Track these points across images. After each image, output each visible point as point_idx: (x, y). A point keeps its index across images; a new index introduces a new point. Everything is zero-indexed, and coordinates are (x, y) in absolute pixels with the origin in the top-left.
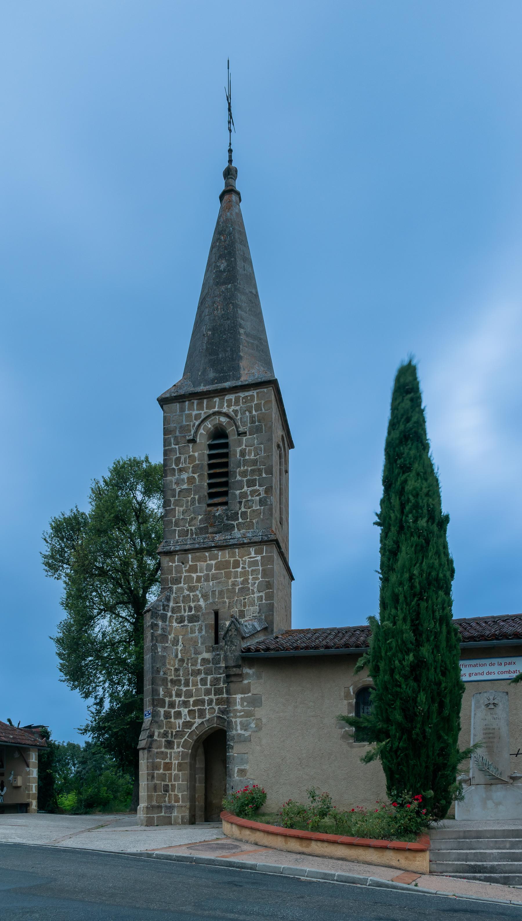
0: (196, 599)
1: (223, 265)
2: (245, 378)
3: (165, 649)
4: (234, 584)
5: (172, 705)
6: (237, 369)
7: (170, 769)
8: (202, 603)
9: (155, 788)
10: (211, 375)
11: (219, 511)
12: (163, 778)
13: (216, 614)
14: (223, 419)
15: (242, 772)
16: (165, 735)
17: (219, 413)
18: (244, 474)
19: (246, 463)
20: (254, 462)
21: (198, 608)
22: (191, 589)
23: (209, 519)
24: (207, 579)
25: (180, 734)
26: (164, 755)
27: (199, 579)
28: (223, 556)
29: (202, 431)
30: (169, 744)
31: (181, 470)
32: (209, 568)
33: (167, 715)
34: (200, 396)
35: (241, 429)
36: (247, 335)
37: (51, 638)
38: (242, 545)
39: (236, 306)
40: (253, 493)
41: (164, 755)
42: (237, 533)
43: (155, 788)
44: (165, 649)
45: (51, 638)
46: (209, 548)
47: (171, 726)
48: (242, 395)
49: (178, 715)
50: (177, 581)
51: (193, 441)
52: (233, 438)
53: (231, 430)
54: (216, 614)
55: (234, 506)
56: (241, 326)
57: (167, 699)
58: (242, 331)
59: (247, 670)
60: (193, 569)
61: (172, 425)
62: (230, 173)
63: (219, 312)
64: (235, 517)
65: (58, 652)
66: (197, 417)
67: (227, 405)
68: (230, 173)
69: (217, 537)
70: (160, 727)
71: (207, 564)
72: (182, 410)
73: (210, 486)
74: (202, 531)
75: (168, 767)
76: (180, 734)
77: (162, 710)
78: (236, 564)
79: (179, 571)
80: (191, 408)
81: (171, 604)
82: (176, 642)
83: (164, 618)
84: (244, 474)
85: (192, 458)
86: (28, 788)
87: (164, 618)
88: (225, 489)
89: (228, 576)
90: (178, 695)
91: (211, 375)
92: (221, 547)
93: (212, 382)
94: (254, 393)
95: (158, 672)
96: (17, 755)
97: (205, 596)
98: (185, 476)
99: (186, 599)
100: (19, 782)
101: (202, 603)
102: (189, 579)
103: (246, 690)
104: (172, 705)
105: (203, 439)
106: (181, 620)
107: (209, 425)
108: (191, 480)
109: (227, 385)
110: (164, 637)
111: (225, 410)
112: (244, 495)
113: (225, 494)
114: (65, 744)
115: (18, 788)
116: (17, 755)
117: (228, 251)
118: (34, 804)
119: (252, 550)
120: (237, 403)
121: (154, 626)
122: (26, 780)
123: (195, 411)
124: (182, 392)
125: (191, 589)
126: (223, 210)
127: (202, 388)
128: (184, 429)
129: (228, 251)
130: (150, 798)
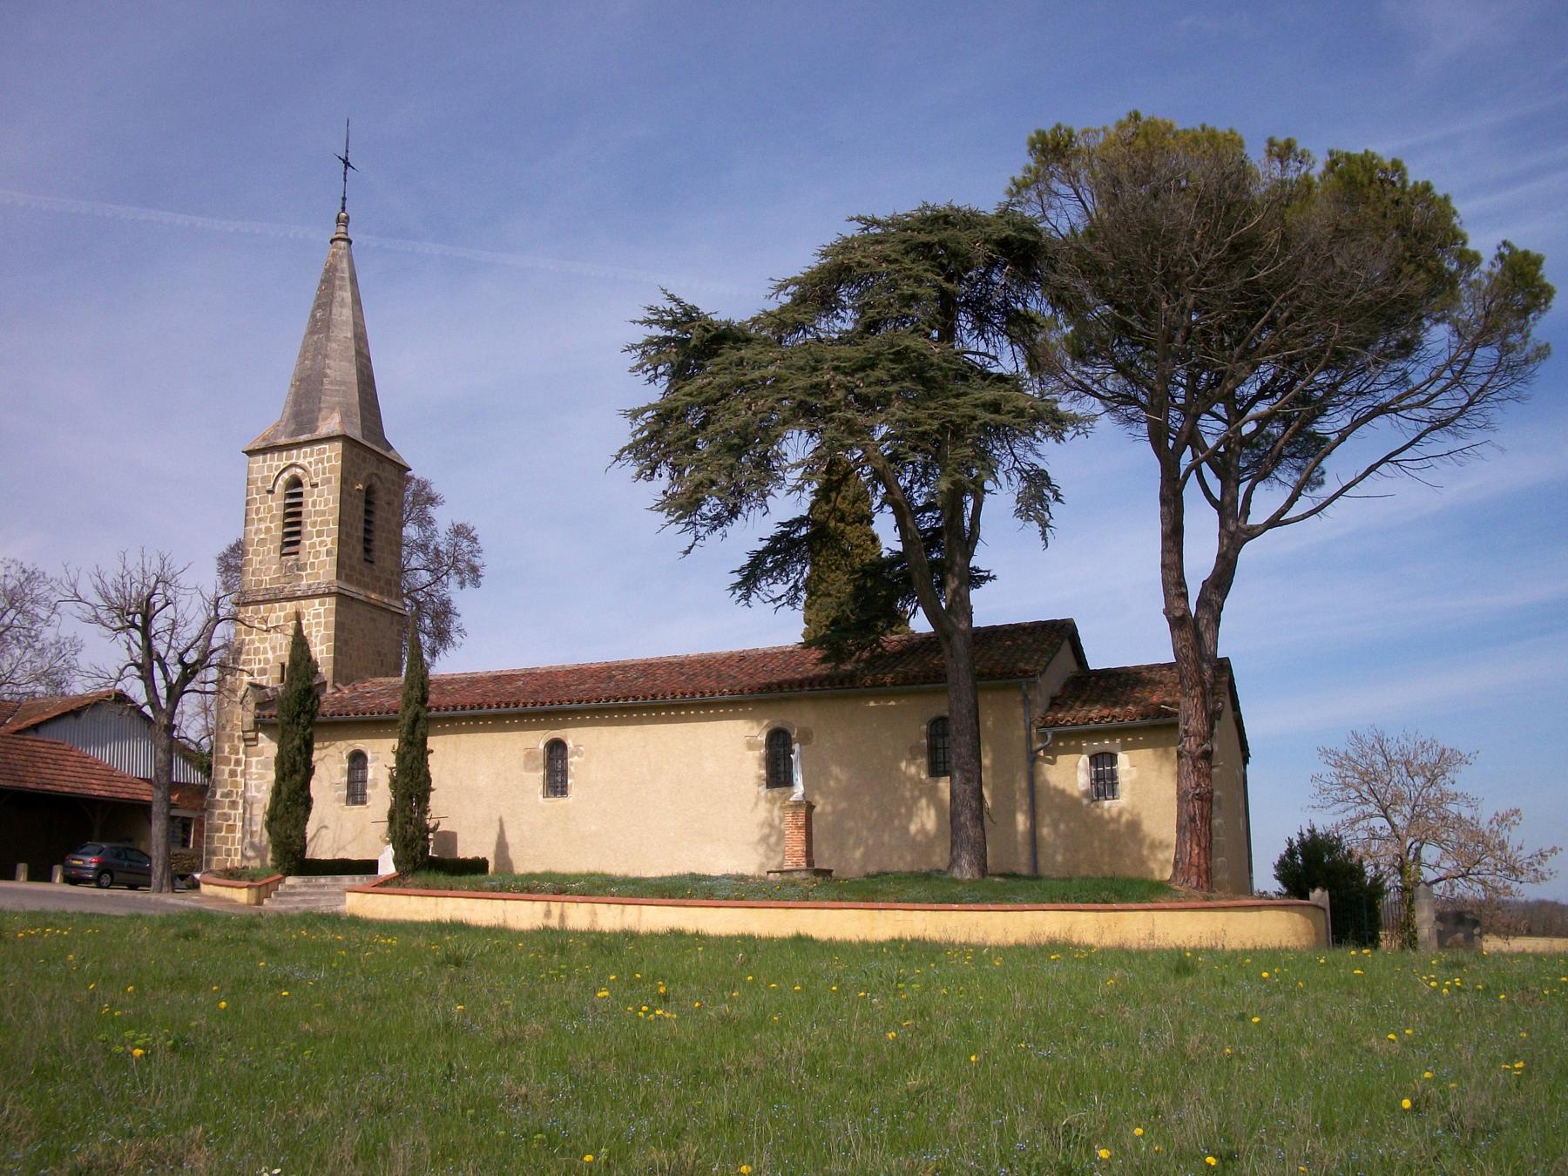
0: (265, 652)
7: (233, 831)
8: (270, 655)
14: (299, 471)
17: (292, 465)
18: (314, 524)
20: (323, 513)
21: (267, 661)
29: (280, 482)
31: (260, 520)
32: (278, 619)
35: (314, 480)
37: (687, 552)
45: (687, 552)
46: (278, 600)
52: (306, 488)
53: (305, 480)
55: (303, 557)
56: (326, 376)
57: (233, 757)
62: (665, 292)
65: (185, 617)
77: (227, 769)
85: (270, 509)
88: (286, 550)
95: (224, 728)
97: (273, 649)
98: (263, 526)
101: (270, 655)
107: (286, 475)
108: (268, 530)
109: (303, 438)
111: (300, 462)
112: (313, 546)
119: (317, 601)
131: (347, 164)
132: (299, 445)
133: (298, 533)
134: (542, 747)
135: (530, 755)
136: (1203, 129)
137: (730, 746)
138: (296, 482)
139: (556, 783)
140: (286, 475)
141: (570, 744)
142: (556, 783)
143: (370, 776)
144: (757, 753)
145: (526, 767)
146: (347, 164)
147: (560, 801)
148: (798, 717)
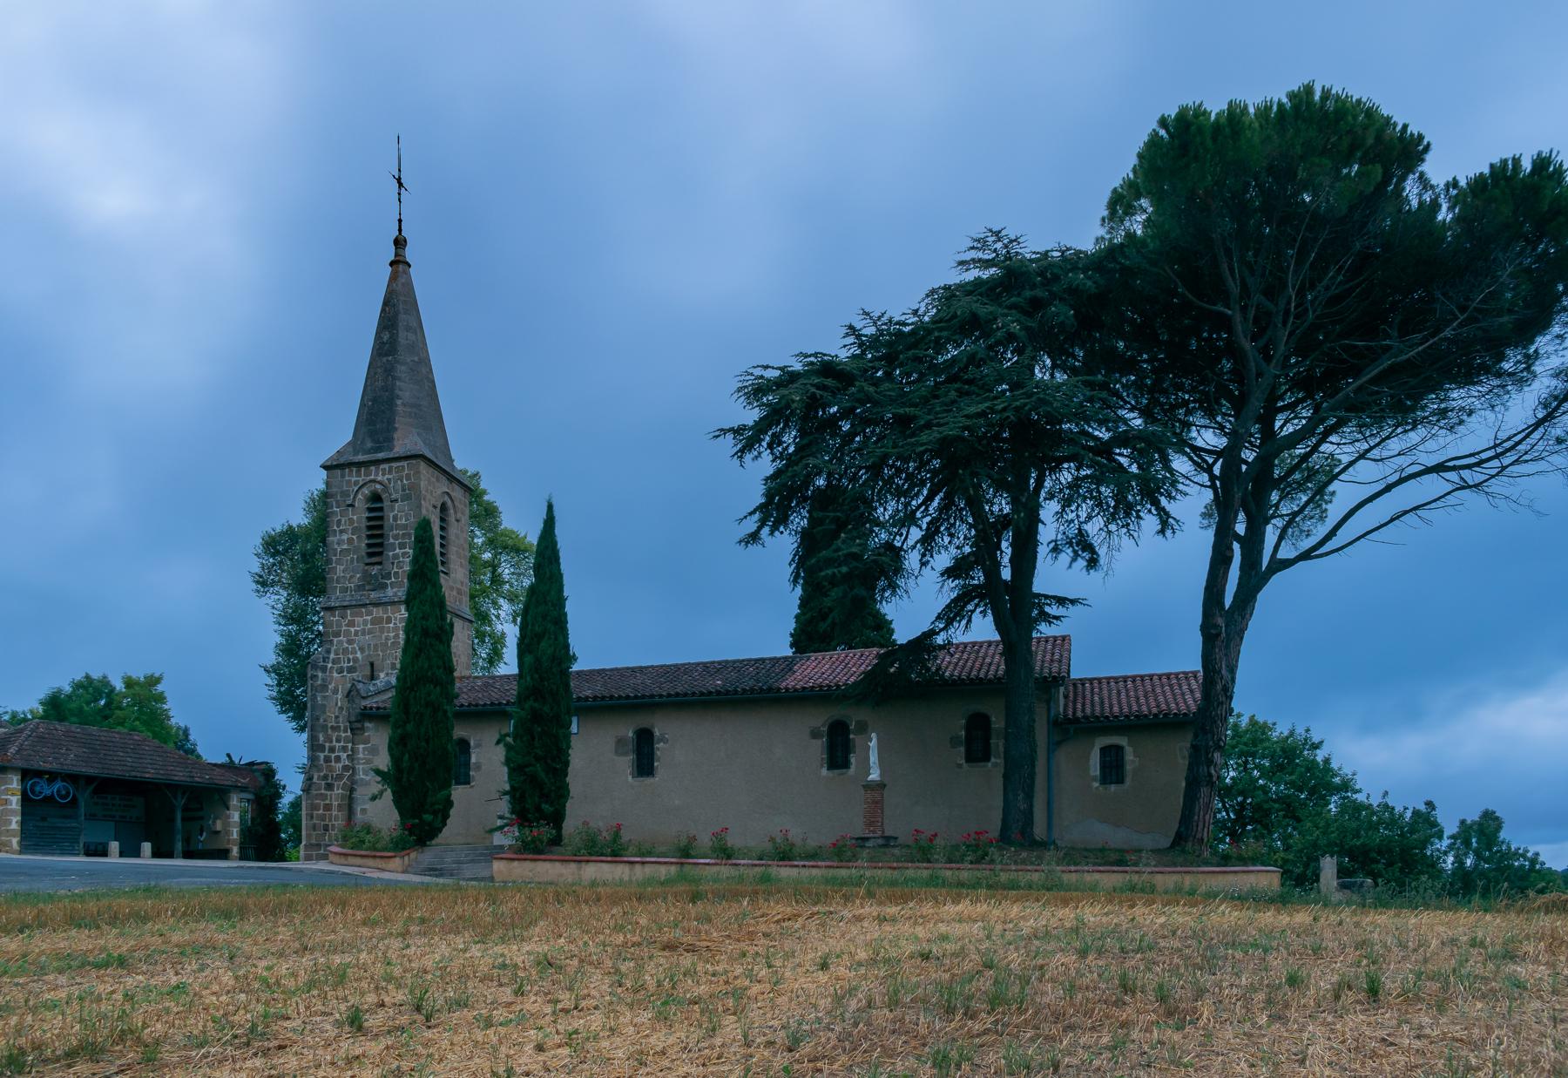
1: (386, 337)
2: (399, 448)
3: (324, 697)
4: (387, 639)
5: (332, 750)
6: (390, 440)
8: (359, 655)
9: (314, 827)
10: (369, 445)
11: (375, 570)
12: (323, 818)
13: (372, 665)
15: (364, 811)
16: (325, 777)
17: (374, 481)
18: (396, 537)
19: (398, 527)
20: (405, 527)
21: (356, 660)
22: (350, 642)
23: (367, 577)
24: (364, 633)
25: (339, 777)
26: (324, 797)
27: (356, 633)
28: (377, 612)
30: (329, 787)
33: (327, 760)
34: (359, 464)
36: (404, 405)
38: (393, 603)
39: (394, 378)
40: (404, 554)
41: (324, 797)
42: (390, 592)
43: (314, 827)
44: (324, 697)
46: (364, 605)
47: (331, 769)
48: (394, 465)
49: (338, 759)
50: (337, 634)
51: (352, 505)
52: (386, 504)
54: (372, 665)
55: (387, 566)
56: (398, 397)
58: (399, 402)
59: (367, 724)
60: (351, 624)
61: (334, 490)
62: (400, 243)
63: (380, 384)
64: (388, 576)
66: (356, 483)
67: (381, 475)
68: (400, 243)
69: (373, 595)
70: (320, 770)
71: (363, 620)
72: (343, 476)
73: (369, 546)
74: (359, 588)
75: (328, 807)
76: (339, 777)
77: (322, 755)
78: (389, 620)
79: (339, 625)
80: (350, 474)
81: (332, 656)
82: (336, 691)
83: (324, 669)
84: (396, 537)
86: (228, 833)
87: (324, 669)
89: (382, 630)
90: (338, 741)
91: (369, 445)
92: (376, 605)
93: (369, 452)
94: (405, 463)
96: (217, 797)
97: (362, 650)
98: (345, 537)
99: (346, 651)
100: (219, 826)
101: (359, 655)
102: (347, 633)
103: (366, 741)
104: (332, 750)
105: (361, 502)
106: (340, 671)
107: (366, 491)
108: (350, 541)
109: (381, 455)
110: (324, 687)
112: (396, 556)
113: (381, 553)
114: (1408, 814)
115: (218, 833)
116: (217, 797)
117: (397, 323)
118: (235, 851)
120: (390, 472)
121: (314, 677)
122: (227, 824)
123: (354, 478)
124: (342, 461)
125: (350, 642)
126: (394, 278)
127: (361, 458)
128: (345, 494)
129: (397, 323)
130: (308, 836)
131: (400, 185)
132: (377, 462)
133: (381, 545)
134: (631, 734)
135: (620, 742)
136: (1210, 516)
137: (792, 742)
138: (376, 497)
139: (645, 766)
140: (366, 491)
141: (657, 733)
142: (645, 766)
143: (473, 760)
144: (819, 742)
145: (617, 753)
146: (400, 185)
147: (649, 781)
148: (854, 716)
